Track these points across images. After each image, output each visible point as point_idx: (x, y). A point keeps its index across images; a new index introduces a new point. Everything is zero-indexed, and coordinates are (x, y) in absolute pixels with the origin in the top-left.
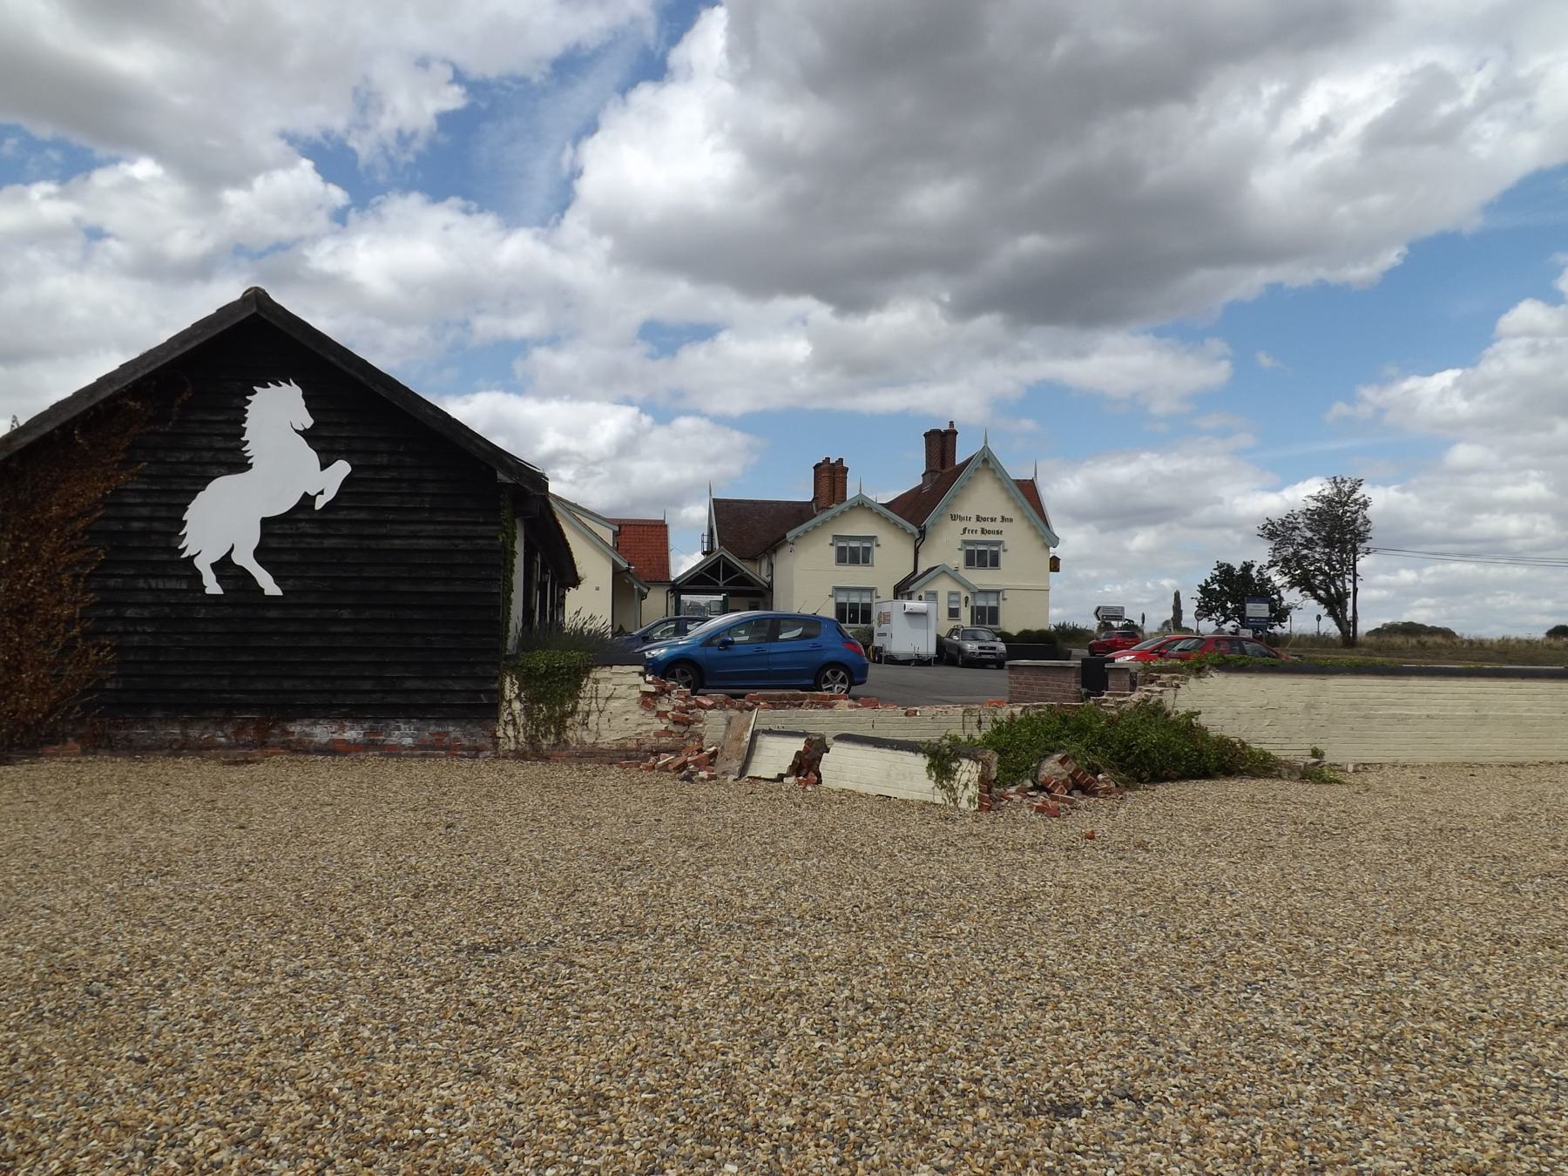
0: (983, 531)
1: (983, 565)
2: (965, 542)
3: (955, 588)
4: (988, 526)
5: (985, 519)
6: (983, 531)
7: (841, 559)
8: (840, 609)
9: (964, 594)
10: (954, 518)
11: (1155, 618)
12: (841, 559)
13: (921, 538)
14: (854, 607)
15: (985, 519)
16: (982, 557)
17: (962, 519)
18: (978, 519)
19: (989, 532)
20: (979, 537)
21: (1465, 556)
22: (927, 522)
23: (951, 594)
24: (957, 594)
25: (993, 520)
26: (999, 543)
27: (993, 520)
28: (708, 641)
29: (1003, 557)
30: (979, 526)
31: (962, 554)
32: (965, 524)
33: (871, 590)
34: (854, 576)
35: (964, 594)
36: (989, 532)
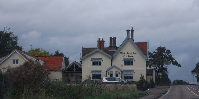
0: (129, 56)
1: (129, 64)
2: (124, 59)
3: (117, 70)
4: (130, 55)
5: (129, 53)
6: (129, 56)
7: (94, 64)
8: (93, 76)
9: (119, 71)
10: (121, 53)
11: (53, 54)
12: (94, 64)
13: (112, 59)
14: (97, 75)
15: (129, 53)
16: (129, 62)
17: (123, 53)
18: (127, 53)
19: (130, 56)
20: (128, 58)
21: (26, 58)
22: (114, 55)
23: (116, 72)
24: (118, 72)
25: (131, 53)
26: (133, 59)
27: (131, 53)
28: (71, 87)
29: (134, 62)
30: (127, 55)
31: (123, 62)
32: (124, 55)
33: (100, 71)
34: (97, 68)
35: (119, 71)
36: (130, 56)
